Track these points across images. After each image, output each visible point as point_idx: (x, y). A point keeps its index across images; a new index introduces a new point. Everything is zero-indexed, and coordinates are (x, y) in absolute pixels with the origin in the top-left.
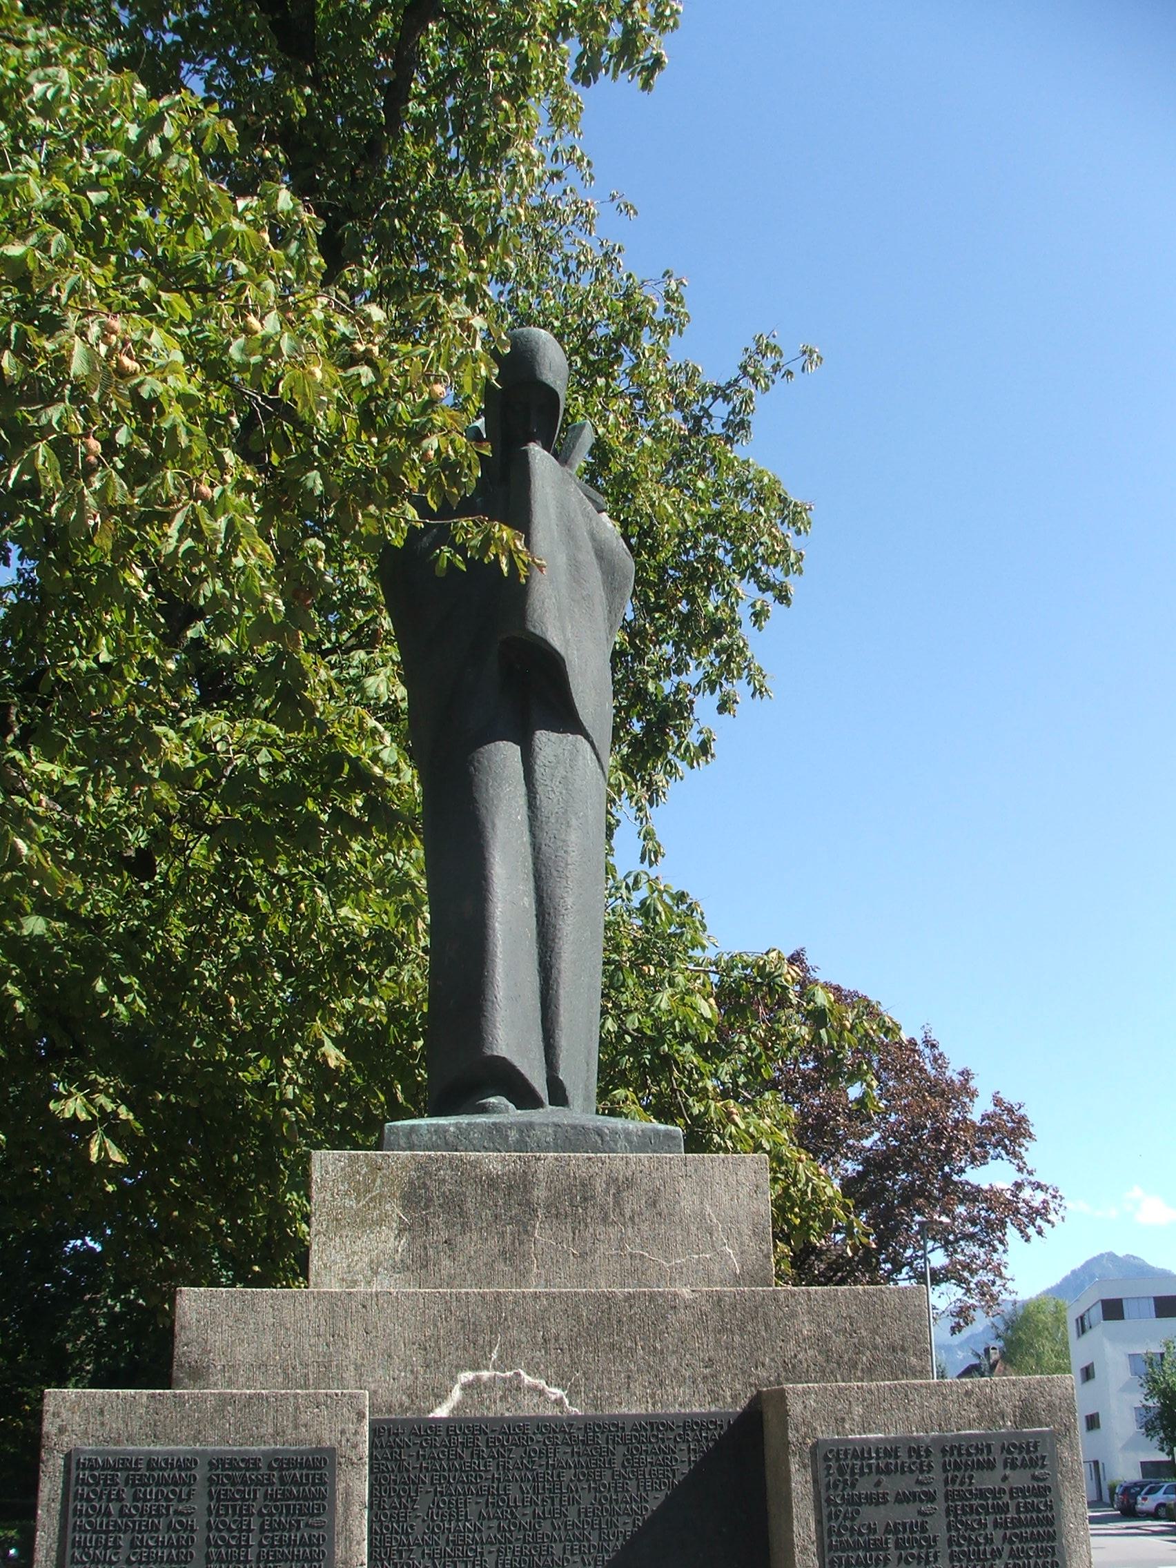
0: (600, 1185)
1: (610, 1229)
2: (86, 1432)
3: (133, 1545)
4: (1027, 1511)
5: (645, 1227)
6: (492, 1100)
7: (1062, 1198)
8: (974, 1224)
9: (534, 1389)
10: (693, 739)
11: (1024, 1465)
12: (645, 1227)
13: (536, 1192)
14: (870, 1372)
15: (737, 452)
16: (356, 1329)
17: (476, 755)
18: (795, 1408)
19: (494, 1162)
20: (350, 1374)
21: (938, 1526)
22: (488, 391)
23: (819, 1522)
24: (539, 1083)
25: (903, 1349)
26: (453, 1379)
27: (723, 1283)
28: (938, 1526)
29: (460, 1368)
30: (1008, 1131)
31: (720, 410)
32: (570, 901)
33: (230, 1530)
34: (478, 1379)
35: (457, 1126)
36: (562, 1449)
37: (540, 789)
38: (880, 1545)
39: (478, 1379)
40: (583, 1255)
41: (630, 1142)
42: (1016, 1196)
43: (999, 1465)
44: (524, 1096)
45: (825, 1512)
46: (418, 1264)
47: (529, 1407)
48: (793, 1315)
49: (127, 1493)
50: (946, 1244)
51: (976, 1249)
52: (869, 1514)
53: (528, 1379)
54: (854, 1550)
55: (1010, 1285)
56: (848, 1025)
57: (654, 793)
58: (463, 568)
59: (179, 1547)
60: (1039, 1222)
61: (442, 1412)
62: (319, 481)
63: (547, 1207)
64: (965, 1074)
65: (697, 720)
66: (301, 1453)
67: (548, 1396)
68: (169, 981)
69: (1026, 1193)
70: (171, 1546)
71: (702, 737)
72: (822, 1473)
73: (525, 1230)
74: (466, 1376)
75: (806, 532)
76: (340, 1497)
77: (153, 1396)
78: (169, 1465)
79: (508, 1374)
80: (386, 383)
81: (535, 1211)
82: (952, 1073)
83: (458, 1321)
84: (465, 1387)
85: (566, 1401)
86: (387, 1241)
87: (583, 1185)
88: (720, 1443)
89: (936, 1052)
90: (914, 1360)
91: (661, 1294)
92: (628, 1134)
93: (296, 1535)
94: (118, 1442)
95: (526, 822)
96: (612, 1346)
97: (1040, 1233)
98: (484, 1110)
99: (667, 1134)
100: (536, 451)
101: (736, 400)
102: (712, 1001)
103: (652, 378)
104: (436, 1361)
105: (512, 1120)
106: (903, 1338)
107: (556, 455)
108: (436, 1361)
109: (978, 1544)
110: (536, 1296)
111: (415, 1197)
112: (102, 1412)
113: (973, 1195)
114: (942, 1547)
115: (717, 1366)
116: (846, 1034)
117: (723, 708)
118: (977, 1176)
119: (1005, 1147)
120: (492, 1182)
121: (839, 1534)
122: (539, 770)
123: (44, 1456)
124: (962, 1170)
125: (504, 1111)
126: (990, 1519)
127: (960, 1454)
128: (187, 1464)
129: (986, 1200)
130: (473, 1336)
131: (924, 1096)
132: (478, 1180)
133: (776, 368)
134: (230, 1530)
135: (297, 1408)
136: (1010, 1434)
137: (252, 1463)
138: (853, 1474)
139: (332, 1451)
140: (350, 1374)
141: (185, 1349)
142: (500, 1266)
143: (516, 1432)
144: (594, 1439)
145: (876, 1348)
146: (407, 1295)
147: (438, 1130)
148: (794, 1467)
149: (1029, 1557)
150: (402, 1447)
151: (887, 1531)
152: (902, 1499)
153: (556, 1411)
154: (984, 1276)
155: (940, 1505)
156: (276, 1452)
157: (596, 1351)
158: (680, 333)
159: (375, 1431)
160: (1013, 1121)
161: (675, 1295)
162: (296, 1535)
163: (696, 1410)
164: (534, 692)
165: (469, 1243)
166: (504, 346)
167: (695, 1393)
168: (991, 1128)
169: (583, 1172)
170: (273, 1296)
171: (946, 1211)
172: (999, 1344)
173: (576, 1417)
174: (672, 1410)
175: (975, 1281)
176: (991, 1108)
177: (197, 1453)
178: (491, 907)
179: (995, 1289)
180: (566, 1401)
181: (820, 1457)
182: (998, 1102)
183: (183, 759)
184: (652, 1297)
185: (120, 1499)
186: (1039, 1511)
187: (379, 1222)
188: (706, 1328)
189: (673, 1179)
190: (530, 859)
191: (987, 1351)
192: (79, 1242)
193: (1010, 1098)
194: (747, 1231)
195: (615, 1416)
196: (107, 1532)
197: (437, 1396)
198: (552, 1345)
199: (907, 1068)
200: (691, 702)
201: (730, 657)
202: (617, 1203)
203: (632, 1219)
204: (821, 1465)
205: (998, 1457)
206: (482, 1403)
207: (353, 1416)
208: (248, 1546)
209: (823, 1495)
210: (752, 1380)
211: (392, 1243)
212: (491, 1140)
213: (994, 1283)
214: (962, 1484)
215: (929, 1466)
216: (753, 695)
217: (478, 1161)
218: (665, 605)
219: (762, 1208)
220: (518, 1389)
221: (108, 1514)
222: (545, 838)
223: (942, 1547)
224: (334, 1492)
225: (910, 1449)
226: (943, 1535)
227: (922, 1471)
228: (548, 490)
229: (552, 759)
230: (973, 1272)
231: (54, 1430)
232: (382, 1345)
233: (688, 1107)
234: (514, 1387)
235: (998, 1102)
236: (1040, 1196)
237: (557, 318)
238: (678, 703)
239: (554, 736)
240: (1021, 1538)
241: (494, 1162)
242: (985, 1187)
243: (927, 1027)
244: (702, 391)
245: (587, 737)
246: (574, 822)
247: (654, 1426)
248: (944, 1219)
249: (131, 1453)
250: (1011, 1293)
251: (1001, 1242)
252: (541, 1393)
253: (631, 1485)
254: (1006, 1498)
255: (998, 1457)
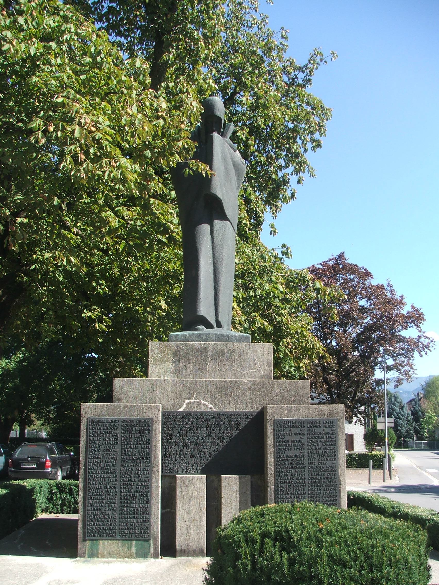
0: (226, 351)
1: (229, 363)
2: (91, 413)
3: (103, 440)
4: (329, 438)
5: (238, 362)
6: (199, 327)
7: (435, 342)
8: (403, 350)
9: (204, 404)
10: (289, 193)
11: (329, 427)
12: (238, 362)
13: (209, 353)
14: (294, 402)
15: (308, 90)
16: (159, 389)
17: (197, 228)
18: (269, 411)
19: (197, 345)
20: (157, 400)
21: (305, 441)
22: (202, 114)
23: (274, 439)
24: (213, 322)
25: (303, 397)
26: (184, 402)
27: (259, 378)
28: (305, 441)
29: (186, 399)
30: (416, 318)
31: (301, 76)
32: (223, 270)
33: (127, 437)
34: (190, 402)
35: (189, 334)
36: (211, 420)
37: (215, 238)
38: (289, 446)
39: (190, 402)
40: (221, 370)
41: (236, 339)
42: (418, 340)
43: (322, 427)
44: (208, 325)
45: (276, 437)
46: (177, 372)
47: (203, 409)
48: (274, 387)
49: (102, 428)
50: (393, 357)
51: (404, 359)
52: (288, 438)
53: (203, 402)
54: (283, 446)
55: (416, 372)
56: (327, 293)
57: (277, 209)
58: (192, 174)
59: (115, 441)
60: (426, 350)
61: (181, 410)
62: (150, 154)
63: (212, 357)
64: (402, 297)
65: (290, 186)
66: (144, 419)
67: (208, 406)
68: (114, 283)
69: (422, 340)
70: (113, 441)
71: (292, 192)
72: (276, 427)
73: (205, 363)
74: (187, 401)
75: (330, 119)
76: (154, 430)
77: (108, 405)
78: (112, 422)
79: (198, 401)
80: (168, 124)
81: (208, 358)
82: (397, 297)
83: (185, 387)
84: (187, 404)
85: (213, 408)
86: (169, 366)
87: (222, 351)
88: (252, 419)
89: (392, 289)
90: (306, 400)
91: (239, 381)
92: (235, 337)
93: (143, 439)
94: (99, 416)
95: (211, 247)
96: (225, 394)
97: (426, 354)
98: (197, 329)
99: (246, 337)
100: (216, 135)
101: (307, 71)
102: (284, 286)
103: (275, 68)
104: (180, 397)
105: (204, 333)
106: (303, 394)
107: (222, 136)
108: (180, 397)
109: (315, 446)
110: (206, 381)
111: (177, 354)
112: (95, 409)
113: (403, 340)
114: (306, 446)
115: (253, 400)
116: (327, 296)
117: (299, 182)
118: (405, 333)
119: (414, 323)
120: (197, 350)
121: (279, 442)
122: (215, 232)
123: (82, 419)
124: (399, 331)
125: (203, 330)
126: (319, 440)
127: (312, 424)
128: (116, 421)
129: (407, 342)
130: (189, 391)
131: (386, 305)
132: (193, 350)
133: (321, 60)
134: (127, 437)
135: (143, 408)
136: (326, 419)
137: (132, 421)
138: (284, 428)
139: (152, 419)
140: (157, 400)
141: (116, 393)
142: (199, 372)
143: (200, 415)
144: (220, 418)
145: (295, 396)
146: (172, 380)
147: (184, 335)
148: (268, 426)
149: (328, 449)
150: (170, 419)
151: (292, 442)
152: (296, 434)
153: (210, 410)
154: (406, 368)
155: (306, 436)
156: (138, 419)
157: (221, 395)
158: (285, 52)
159: (163, 414)
160: (418, 314)
161: (242, 381)
162: (143, 439)
163: (247, 411)
164: (214, 209)
165: (191, 366)
166: (202, 110)
167: (246, 407)
168: (410, 317)
169: (221, 348)
170: (138, 380)
171: (392, 346)
172: (422, 392)
173: (215, 412)
174: (240, 411)
175: (403, 370)
176: (410, 310)
177: (118, 419)
178: (200, 273)
179: (410, 373)
180: (213, 408)
181: (275, 423)
182: (413, 307)
183: (115, 223)
184: (236, 382)
185: (100, 429)
186: (332, 438)
187: (167, 361)
188: (250, 390)
189: (246, 350)
190: (212, 258)
191: (418, 394)
192: (90, 355)
193: (417, 306)
194: (266, 364)
195: (226, 412)
196: (97, 437)
197: (180, 406)
198: (209, 394)
199: (380, 295)
200: (289, 179)
201: (301, 165)
202: (231, 356)
203: (234, 360)
204: (276, 425)
205: (322, 425)
206: (191, 408)
207: (157, 410)
208: (131, 441)
209: (276, 433)
210: (262, 403)
211: (170, 366)
212: (198, 338)
213: (410, 371)
214: (312, 431)
215: (304, 426)
216: (310, 177)
217: (193, 344)
218: (280, 146)
219: (270, 358)
220: (201, 404)
221: (97, 433)
222: (216, 252)
223: (306, 446)
224: (152, 428)
225: (299, 422)
226: (306, 443)
227: (302, 428)
228: (218, 147)
229: (219, 228)
230: (403, 367)
231: (84, 413)
232: (166, 393)
233: (276, 319)
234: (200, 404)
235: (413, 307)
236: (427, 341)
237: (243, 46)
238: (284, 180)
239: (219, 221)
240: (327, 445)
241: (197, 345)
242: (407, 337)
243: (389, 280)
244: (295, 69)
245: (229, 221)
246: (225, 247)
247: (235, 414)
248: (391, 348)
249: (103, 419)
250: (416, 374)
251: (412, 357)
252: (207, 405)
253: (229, 429)
254: (324, 435)
255: (322, 425)
